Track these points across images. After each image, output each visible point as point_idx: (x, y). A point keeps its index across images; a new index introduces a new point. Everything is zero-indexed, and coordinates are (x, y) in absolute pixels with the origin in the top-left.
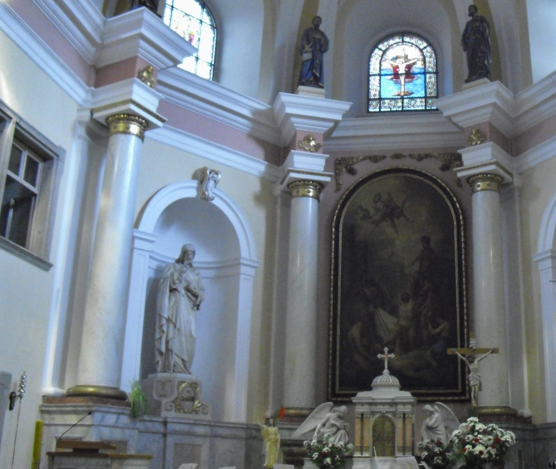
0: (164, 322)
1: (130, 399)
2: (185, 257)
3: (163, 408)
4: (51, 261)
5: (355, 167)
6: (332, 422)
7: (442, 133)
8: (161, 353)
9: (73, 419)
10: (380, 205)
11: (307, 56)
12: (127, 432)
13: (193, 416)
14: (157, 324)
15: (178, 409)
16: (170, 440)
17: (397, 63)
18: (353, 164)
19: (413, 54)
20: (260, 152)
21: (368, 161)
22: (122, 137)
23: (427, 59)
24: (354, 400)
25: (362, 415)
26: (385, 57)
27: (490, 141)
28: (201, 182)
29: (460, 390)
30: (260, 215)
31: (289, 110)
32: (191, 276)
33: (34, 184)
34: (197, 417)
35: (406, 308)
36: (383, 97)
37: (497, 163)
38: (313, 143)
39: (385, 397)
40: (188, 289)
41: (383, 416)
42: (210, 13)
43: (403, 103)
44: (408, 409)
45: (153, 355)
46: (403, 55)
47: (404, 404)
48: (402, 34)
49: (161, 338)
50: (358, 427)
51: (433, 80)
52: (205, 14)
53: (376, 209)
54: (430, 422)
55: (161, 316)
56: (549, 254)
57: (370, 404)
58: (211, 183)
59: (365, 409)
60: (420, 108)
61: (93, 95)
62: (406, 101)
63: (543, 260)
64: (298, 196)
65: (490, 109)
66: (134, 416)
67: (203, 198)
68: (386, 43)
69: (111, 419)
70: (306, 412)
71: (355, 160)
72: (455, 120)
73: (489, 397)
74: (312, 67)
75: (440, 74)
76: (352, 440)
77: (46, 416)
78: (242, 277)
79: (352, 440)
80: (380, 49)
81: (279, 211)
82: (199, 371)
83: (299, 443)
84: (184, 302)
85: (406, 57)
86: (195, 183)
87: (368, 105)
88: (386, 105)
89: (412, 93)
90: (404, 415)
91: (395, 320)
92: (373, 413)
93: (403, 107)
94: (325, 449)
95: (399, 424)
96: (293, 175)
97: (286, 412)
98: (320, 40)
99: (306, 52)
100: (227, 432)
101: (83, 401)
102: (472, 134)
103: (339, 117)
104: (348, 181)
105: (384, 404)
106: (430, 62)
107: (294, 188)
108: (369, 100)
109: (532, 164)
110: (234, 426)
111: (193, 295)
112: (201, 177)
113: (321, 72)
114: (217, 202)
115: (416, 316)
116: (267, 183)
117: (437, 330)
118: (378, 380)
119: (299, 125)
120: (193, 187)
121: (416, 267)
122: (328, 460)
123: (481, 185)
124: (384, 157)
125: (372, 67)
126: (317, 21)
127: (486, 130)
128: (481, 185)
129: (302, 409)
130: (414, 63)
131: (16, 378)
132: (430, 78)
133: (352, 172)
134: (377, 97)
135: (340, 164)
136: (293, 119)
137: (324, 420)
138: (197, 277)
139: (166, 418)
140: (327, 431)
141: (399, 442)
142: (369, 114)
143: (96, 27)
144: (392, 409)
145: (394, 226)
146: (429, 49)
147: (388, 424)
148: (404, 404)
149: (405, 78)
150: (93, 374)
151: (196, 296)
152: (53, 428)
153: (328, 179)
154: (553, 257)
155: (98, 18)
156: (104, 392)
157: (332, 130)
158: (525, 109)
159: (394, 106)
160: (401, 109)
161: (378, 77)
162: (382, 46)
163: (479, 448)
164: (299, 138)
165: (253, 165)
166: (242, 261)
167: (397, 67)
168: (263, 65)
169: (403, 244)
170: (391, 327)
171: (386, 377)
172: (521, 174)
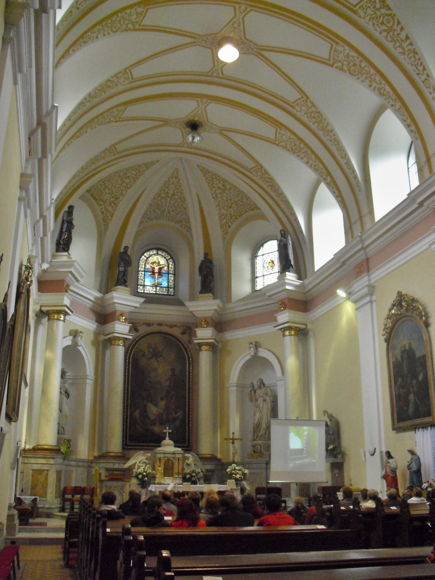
6: (145, 461)
7: (184, 316)
9: (43, 461)
10: (151, 350)
17: (155, 266)
18: (137, 326)
19: (163, 262)
23: (170, 266)
25: (160, 458)
26: (147, 261)
27: (211, 327)
28: (75, 337)
29: (187, 445)
31: (116, 301)
35: (162, 404)
36: (145, 284)
37: (215, 339)
39: (169, 450)
41: (169, 459)
43: (156, 289)
44: (180, 456)
46: (157, 262)
48: (158, 249)
51: (172, 278)
53: (149, 352)
54: (189, 462)
56: (235, 385)
57: (163, 453)
59: (161, 456)
60: (165, 293)
61: (39, 296)
62: (158, 288)
65: (213, 311)
68: (148, 253)
71: (138, 324)
72: (194, 313)
73: (205, 448)
75: (176, 275)
80: (145, 256)
85: (159, 263)
86: (71, 338)
88: (147, 289)
90: (179, 459)
93: (156, 291)
98: (128, 260)
101: (48, 453)
102: (202, 321)
103: (137, 305)
105: (169, 453)
106: (171, 268)
110: (83, 461)
114: (80, 348)
115: (167, 407)
118: (164, 442)
119: (119, 308)
120: (69, 340)
121: (168, 383)
124: (153, 324)
125: (140, 266)
128: (204, 348)
129: (118, 453)
130: (163, 267)
132: (171, 277)
136: (116, 305)
142: (138, 294)
144: (173, 456)
145: (158, 361)
146: (171, 260)
147: (170, 463)
149: (158, 275)
152: (29, 465)
154: (237, 386)
159: (152, 291)
160: (155, 293)
161: (143, 273)
164: (118, 314)
166: (88, 377)
168: (96, 269)
171: (167, 441)
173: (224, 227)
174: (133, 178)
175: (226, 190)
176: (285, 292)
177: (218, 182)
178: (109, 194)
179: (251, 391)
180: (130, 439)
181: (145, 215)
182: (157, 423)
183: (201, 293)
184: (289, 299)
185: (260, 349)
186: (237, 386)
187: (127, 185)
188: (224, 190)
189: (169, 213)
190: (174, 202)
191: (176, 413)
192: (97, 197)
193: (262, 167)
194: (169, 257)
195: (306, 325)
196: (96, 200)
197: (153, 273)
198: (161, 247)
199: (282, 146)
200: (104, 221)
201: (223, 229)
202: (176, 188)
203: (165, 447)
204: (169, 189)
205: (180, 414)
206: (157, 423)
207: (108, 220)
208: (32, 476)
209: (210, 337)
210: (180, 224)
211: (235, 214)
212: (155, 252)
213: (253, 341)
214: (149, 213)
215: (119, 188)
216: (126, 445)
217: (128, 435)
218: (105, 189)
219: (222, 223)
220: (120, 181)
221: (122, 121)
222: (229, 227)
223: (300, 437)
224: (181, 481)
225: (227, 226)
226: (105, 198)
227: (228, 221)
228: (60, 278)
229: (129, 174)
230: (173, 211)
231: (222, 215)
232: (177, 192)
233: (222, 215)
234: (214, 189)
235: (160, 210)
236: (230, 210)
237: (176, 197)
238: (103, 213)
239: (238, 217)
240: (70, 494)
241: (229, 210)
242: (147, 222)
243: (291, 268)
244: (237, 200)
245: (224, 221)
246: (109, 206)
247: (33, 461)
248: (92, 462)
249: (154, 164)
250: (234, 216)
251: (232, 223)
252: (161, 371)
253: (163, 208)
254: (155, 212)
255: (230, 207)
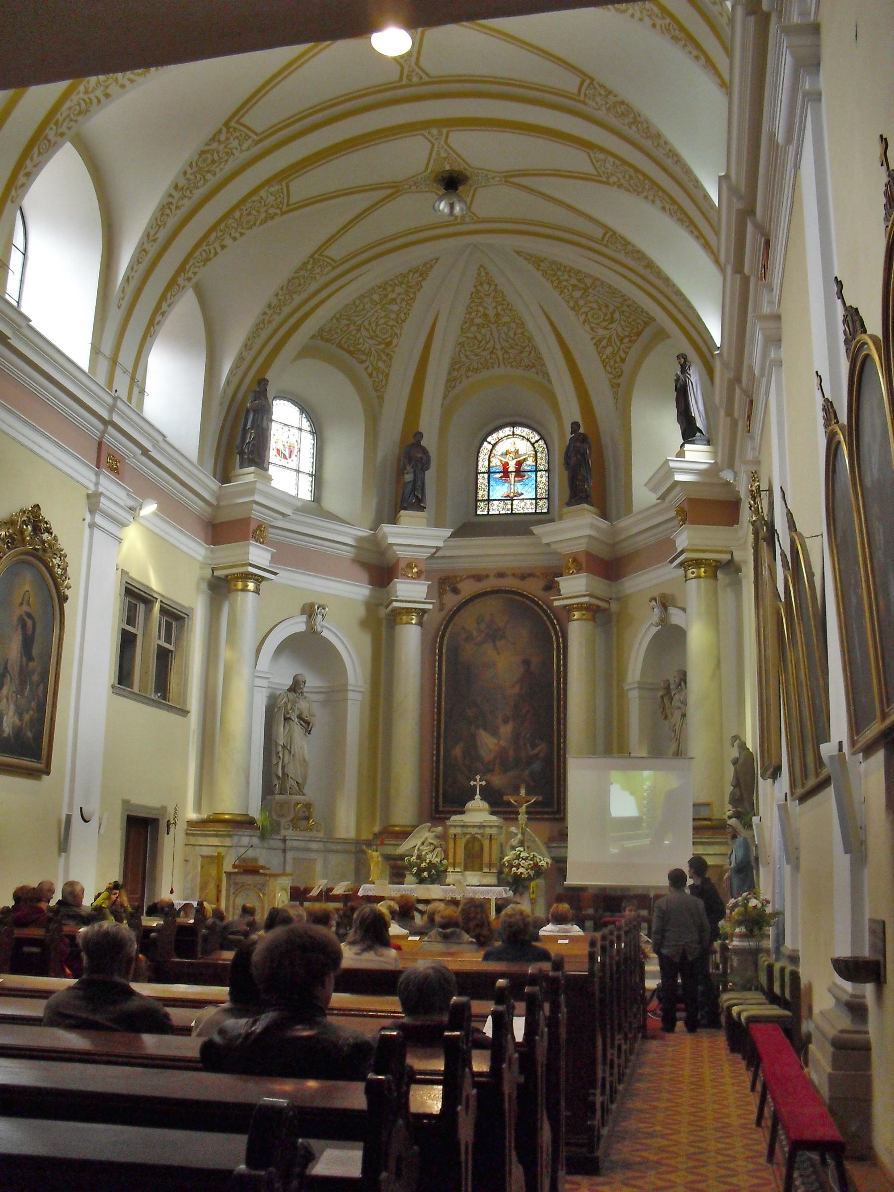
0: (280, 749)
1: (259, 824)
2: (296, 687)
3: (282, 827)
4: (188, 709)
5: (460, 586)
8: (278, 777)
9: (215, 841)
10: (483, 626)
11: (409, 477)
12: (258, 851)
13: (308, 834)
14: (274, 752)
15: (295, 827)
16: (290, 855)
18: (457, 583)
19: (524, 448)
20: (364, 576)
21: (471, 580)
22: (240, 594)
24: (448, 823)
26: (494, 451)
28: (310, 616)
30: (366, 640)
31: (391, 540)
32: (303, 705)
33: (170, 643)
34: (312, 834)
35: (506, 730)
38: (415, 570)
40: (300, 717)
41: (474, 838)
42: (310, 418)
43: (512, 505)
44: (494, 831)
45: (274, 782)
47: (491, 827)
49: (277, 763)
50: (451, 845)
52: (305, 420)
53: (480, 631)
55: (276, 744)
56: (636, 685)
57: (463, 826)
58: (320, 617)
59: (458, 831)
60: (530, 511)
61: (212, 551)
62: (515, 502)
63: (631, 689)
64: (402, 623)
65: (585, 540)
66: (263, 837)
67: (312, 633)
69: (245, 840)
70: (409, 829)
74: (414, 489)
75: (551, 473)
76: (446, 857)
77: (191, 838)
78: (349, 702)
79: (446, 857)
80: (489, 443)
81: (384, 632)
82: (311, 793)
83: (401, 858)
84: (297, 729)
85: (517, 452)
86: (304, 618)
87: (476, 507)
88: (495, 507)
89: (522, 494)
91: (496, 741)
92: (465, 834)
94: (423, 865)
95: (486, 843)
96: (395, 604)
97: (391, 829)
98: (421, 458)
99: (408, 473)
100: (339, 847)
103: (440, 544)
104: (452, 601)
106: (542, 459)
107: (396, 617)
108: (477, 501)
109: (628, 592)
110: (345, 841)
111: (306, 724)
112: (310, 611)
113: (423, 493)
114: (325, 634)
115: (516, 736)
116: (372, 606)
117: (536, 751)
118: (470, 805)
119: (401, 553)
120: (301, 622)
121: (517, 690)
122: (426, 874)
123: (577, 615)
124: (487, 576)
125: (480, 464)
126: (419, 435)
127: (583, 559)
128: (577, 615)
130: (525, 460)
131: (170, 810)
133: (455, 591)
134: (486, 498)
135: (444, 583)
136: (395, 548)
137: (423, 839)
138: (308, 705)
139: (285, 836)
140: (425, 849)
141: (486, 859)
143: (213, 493)
145: (496, 648)
146: (541, 443)
147: (477, 844)
148: (491, 827)
149: (515, 476)
150: (228, 803)
151: (308, 723)
152: (197, 848)
153: (430, 607)
154: (639, 688)
155: (214, 485)
156: (239, 818)
157: (435, 553)
158: (622, 537)
162: (492, 439)
163: (521, 870)
164: (402, 565)
165: (355, 591)
167: (507, 464)
168: (365, 481)
169: (502, 666)
170: (491, 747)
172: (618, 599)
173: (612, 362)
174: (403, 300)
175: (588, 288)
176: (678, 489)
177: (566, 277)
178: (371, 338)
179: (662, 697)
180: (445, 801)
181: (454, 366)
182: (497, 768)
183: (569, 504)
184: (691, 501)
185: (672, 610)
186: (639, 688)
187: (398, 315)
188: (586, 290)
189: (506, 352)
190: (505, 328)
191: (534, 746)
192: (351, 348)
193: (614, 233)
194: (537, 437)
195: (732, 554)
196: (351, 353)
197: (506, 473)
198: (518, 420)
199: (614, 183)
200: (376, 391)
201: (608, 368)
202: (497, 302)
203: (473, 813)
204: (485, 308)
205: (541, 748)
206: (497, 768)
207: (383, 387)
208: (202, 867)
209: (585, 593)
210: (534, 370)
211: (627, 333)
212: (507, 431)
213: (656, 593)
214: (464, 358)
215: (385, 323)
216: (437, 811)
217: (441, 791)
218: (359, 330)
219: (604, 357)
220: (380, 311)
221: (292, 210)
222: (623, 361)
223: (632, 793)
224: (494, 880)
225: (618, 360)
226: (366, 345)
227: (616, 349)
228: (239, 515)
229: (392, 296)
230: (512, 347)
231: (600, 341)
232: (503, 310)
233: (600, 341)
234: (566, 291)
235: (484, 350)
236: (614, 326)
237: (506, 319)
238: (370, 375)
239: (633, 338)
240: (590, 907)
241: (610, 326)
242: (468, 377)
243: (698, 434)
244: (618, 305)
245: (609, 350)
246: (378, 360)
247: (202, 841)
248: (369, 844)
249: (431, 267)
250: (625, 336)
251: (626, 353)
252: (502, 666)
253: (490, 345)
254: (476, 355)
255: (612, 321)
